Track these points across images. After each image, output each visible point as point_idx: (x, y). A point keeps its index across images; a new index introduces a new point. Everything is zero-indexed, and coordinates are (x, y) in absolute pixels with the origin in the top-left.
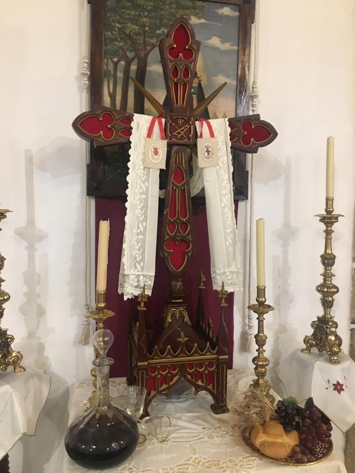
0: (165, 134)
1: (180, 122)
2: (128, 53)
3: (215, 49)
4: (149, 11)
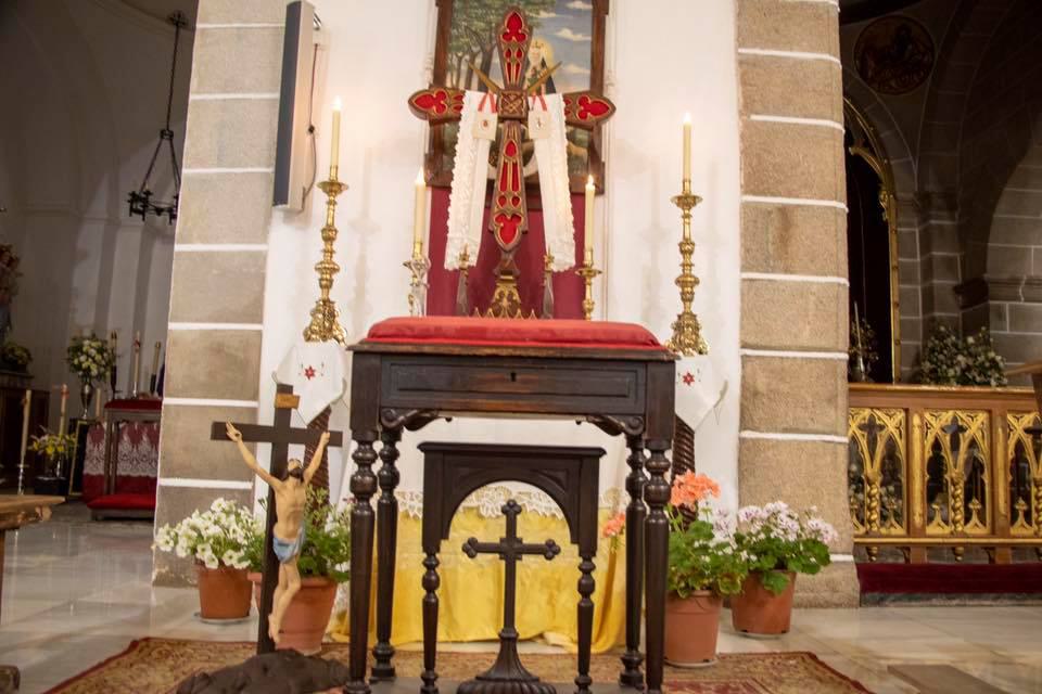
0: (495, 108)
3: (567, 40)
4: (497, 10)
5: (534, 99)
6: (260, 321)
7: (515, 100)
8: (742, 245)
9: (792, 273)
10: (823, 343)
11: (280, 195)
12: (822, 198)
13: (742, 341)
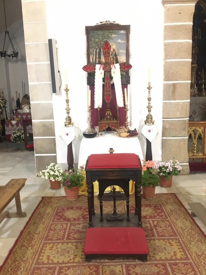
0: (103, 69)
1: (107, 66)
2: (96, 47)
3: (120, 43)
4: (101, 35)
5: (112, 66)
6: (53, 119)
7: (108, 66)
8: (163, 94)
9: (175, 100)
10: (183, 116)
11: (54, 91)
12: (184, 80)
13: (163, 117)
